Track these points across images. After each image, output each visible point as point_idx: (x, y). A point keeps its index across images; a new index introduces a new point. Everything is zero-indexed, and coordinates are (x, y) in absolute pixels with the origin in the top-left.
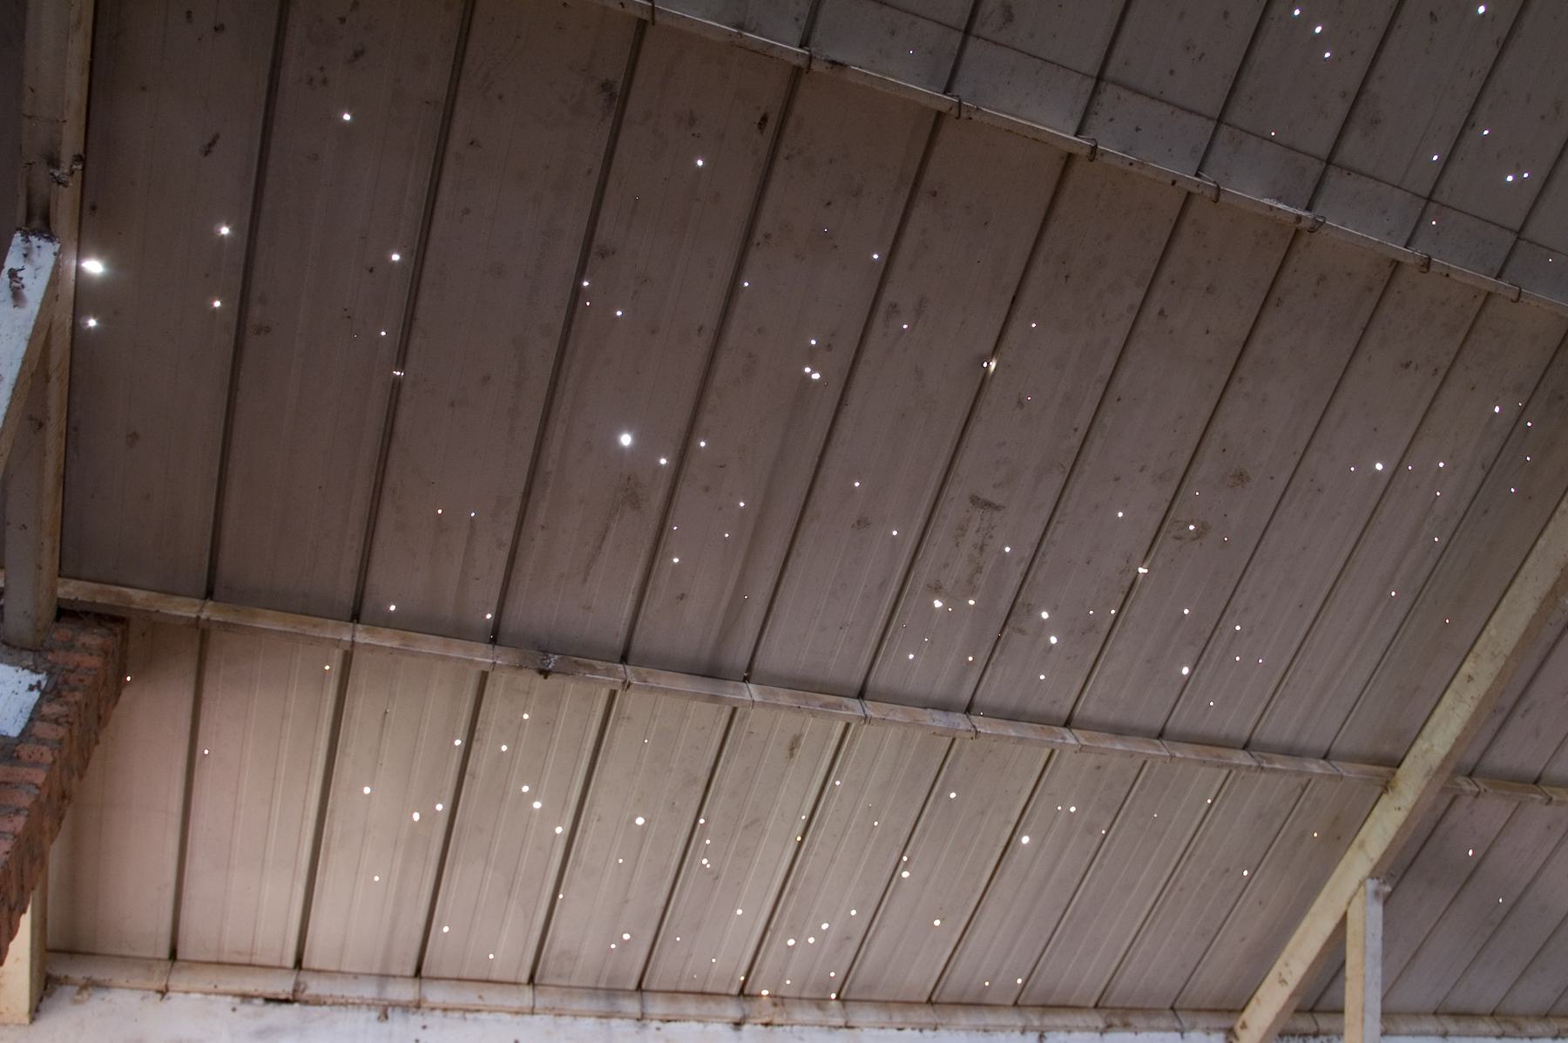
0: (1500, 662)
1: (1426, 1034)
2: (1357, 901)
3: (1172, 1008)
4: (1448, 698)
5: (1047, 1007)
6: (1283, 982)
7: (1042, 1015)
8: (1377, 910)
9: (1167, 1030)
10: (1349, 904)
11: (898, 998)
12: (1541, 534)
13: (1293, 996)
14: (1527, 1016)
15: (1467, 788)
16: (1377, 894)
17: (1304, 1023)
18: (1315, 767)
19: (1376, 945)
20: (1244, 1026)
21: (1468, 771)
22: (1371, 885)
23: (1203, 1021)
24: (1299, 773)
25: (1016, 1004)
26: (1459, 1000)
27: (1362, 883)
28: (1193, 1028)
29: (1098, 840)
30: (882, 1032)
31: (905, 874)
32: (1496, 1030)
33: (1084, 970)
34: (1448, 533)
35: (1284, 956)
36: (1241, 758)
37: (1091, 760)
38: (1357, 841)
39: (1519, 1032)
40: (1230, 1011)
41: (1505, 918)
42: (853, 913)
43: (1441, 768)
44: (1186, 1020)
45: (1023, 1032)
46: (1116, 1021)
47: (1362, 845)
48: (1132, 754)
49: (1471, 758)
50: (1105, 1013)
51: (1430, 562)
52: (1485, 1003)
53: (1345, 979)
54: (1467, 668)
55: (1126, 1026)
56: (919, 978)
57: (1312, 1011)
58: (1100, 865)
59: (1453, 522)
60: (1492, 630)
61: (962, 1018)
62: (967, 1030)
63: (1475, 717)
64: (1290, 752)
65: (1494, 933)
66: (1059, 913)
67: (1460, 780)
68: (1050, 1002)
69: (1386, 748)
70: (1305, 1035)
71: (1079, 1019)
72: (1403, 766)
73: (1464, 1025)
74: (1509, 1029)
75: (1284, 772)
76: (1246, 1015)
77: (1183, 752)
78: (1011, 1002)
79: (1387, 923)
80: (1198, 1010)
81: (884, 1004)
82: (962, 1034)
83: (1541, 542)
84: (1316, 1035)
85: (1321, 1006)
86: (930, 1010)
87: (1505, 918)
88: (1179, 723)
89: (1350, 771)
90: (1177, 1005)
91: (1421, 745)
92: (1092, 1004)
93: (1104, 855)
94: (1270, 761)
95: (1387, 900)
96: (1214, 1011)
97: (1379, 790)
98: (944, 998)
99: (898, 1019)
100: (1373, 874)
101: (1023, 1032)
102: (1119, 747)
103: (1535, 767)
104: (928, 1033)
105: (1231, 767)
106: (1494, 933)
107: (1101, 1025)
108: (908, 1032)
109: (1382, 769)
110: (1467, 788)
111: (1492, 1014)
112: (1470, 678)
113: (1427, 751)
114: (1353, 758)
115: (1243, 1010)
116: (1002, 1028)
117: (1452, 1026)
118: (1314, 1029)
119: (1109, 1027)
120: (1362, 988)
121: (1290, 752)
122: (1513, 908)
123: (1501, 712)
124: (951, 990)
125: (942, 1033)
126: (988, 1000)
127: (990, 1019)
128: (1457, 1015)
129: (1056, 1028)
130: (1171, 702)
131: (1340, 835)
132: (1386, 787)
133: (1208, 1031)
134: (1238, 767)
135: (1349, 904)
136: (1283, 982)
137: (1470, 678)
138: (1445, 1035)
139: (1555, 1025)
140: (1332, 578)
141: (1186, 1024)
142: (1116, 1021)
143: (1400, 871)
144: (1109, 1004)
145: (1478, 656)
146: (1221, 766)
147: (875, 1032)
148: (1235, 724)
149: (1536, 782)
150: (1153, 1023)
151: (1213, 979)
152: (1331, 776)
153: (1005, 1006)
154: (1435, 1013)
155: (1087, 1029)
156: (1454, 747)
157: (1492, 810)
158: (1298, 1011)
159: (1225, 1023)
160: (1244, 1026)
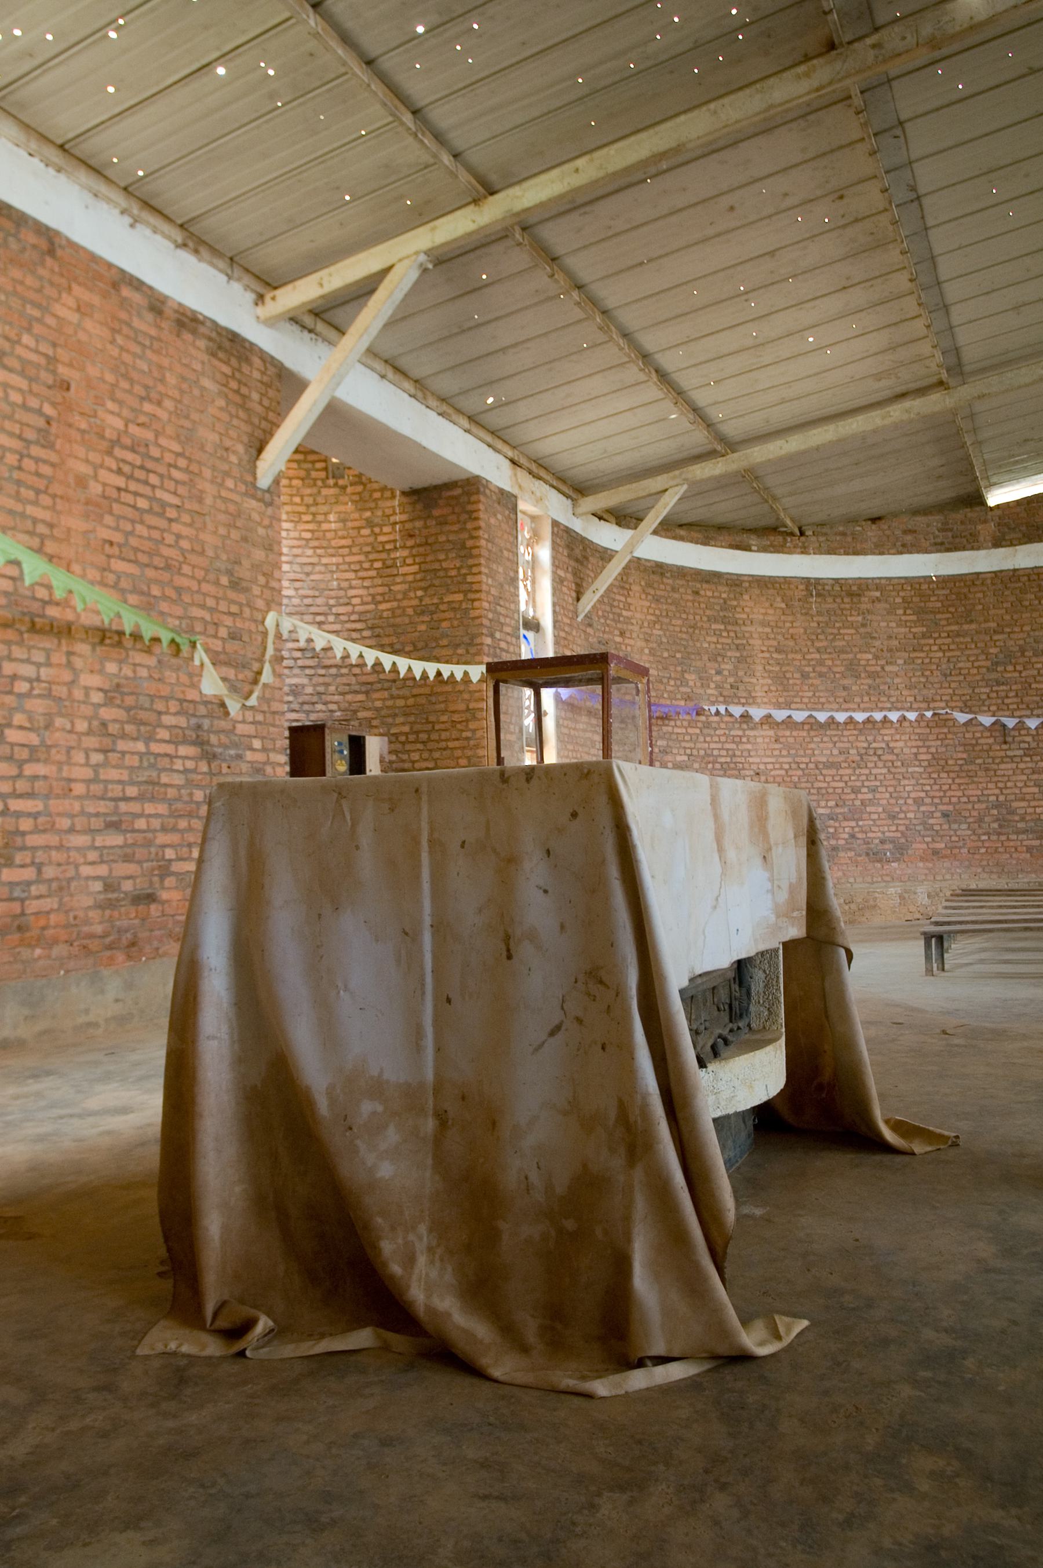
0: (601, 174)
1: (373, 369)
2: (406, 262)
3: (231, 259)
4: (555, 173)
5: (147, 205)
6: (321, 285)
7: (141, 209)
8: (414, 275)
9: (221, 271)
10: (400, 260)
11: (40, 130)
12: (685, 112)
13: (322, 297)
14: (433, 394)
15: (518, 236)
16: (421, 265)
17: (308, 320)
18: (446, 159)
19: (399, 296)
20: (273, 298)
21: (525, 227)
22: (422, 258)
23: (247, 279)
24: (435, 156)
25: (125, 189)
26: (404, 362)
27: (417, 253)
28: (239, 280)
29: (270, 107)
30: (16, 148)
31: (113, 35)
32: (413, 391)
33: (190, 197)
34: (642, 67)
35: (332, 269)
36: (408, 118)
37: (312, 44)
38: (431, 224)
39: (423, 401)
40: (268, 284)
41: (470, 329)
42: (49, 37)
43: (518, 214)
44: (237, 272)
45: (122, 212)
46: (191, 244)
47: (433, 229)
48: (344, 64)
49: (532, 220)
50: (186, 234)
51: (617, 78)
52: (417, 373)
53: (365, 305)
54: (580, 163)
55: (196, 252)
56: (67, 122)
57: (317, 315)
58: (258, 127)
59: (649, 63)
60: (612, 150)
61: (84, 176)
62: (83, 187)
63: (561, 197)
64: (439, 137)
65: (457, 334)
66: (205, 141)
67: (517, 229)
68: (152, 203)
69: (493, 178)
70: (304, 327)
71: (166, 227)
72: (497, 197)
73: (398, 378)
74: (420, 395)
75: (427, 148)
76: (278, 292)
77: (376, 86)
78: (123, 184)
79: (417, 283)
80: (247, 270)
81: (26, 127)
82: (77, 187)
83: (682, 118)
84: (310, 331)
85: (326, 316)
86: (59, 152)
87: (470, 329)
88: (387, 63)
89: (464, 176)
90: (236, 259)
91: (516, 191)
92: (179, 222)
93: (266, 122)
94: (423, 134)
95: (425, 270)
96: (258, 277)
97: (470, 199)
98: (76, 151)
99: (34, 145)
100: (427, 253)
101: (122, 212)
102: (340, 52)
103: (559, 250)
104: (51, 171)
105: (397, 118)
106: (457, 334)
107: (180, 240)
108: (35, 161)
109: (480, 188)
110: (518, 236)
111: (416, 381)
112: (577, 170)
113: (517, 197)
114: (470, 169)
115: (276, 288)
116: (109, 200)
117: (390, 374)
118: (312, 326)
119: (185, 245)
120: (370, 320)
121: (439, 137)
122: (479, 325)
123: (572, 205)
124: (84, 149)
125: (62, 177)
126: (108, 173)
127: (103, 188)
128: (397, 369)
129: (148, 224)
130: (394, 44)
131: (425, 213)
132: (476, 202)
133: (247, 287)
134: (402, 124)
135: (400, 260)
136: (321, 285)
137: (577, 170)
138: (383, 377)
139: (445, 408)
140: (557, 40)
141: (236, 275)
142: (191, 244)
143: (444, 260)
144: (191, 229)
145: (592, 160)
146: (393, 115)
147: (10, 145)
148: (419, 90)
149: (553, 260)
150: (215, 261)
151: (273, 256)
152: (452, 172)
153: (118, 186)
154: (386, 361)
155: (168, 237)
156: (536, 206)
157: (520, 258)
158: (310, 311)
159: (260, 289)
160: (273, 298)
